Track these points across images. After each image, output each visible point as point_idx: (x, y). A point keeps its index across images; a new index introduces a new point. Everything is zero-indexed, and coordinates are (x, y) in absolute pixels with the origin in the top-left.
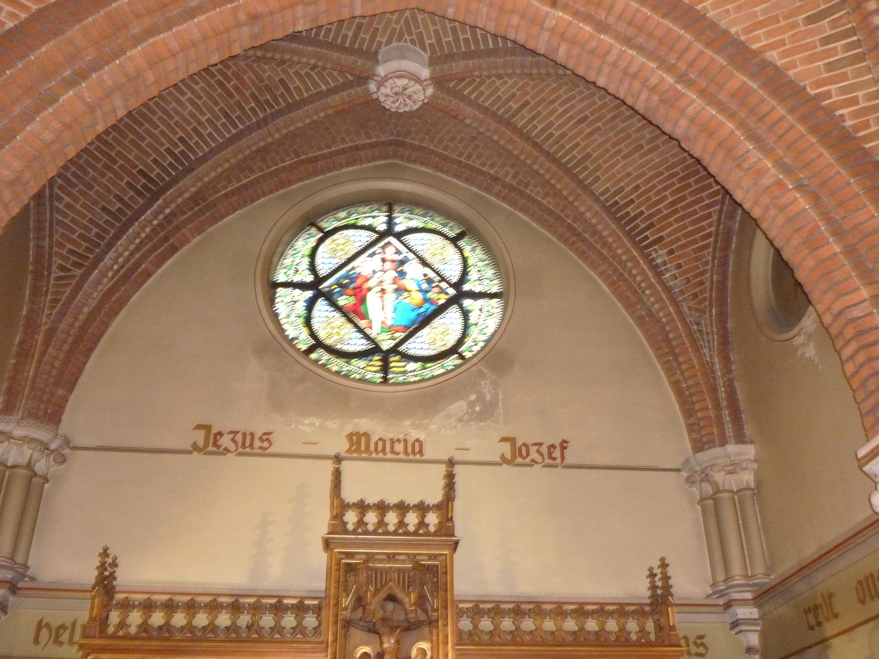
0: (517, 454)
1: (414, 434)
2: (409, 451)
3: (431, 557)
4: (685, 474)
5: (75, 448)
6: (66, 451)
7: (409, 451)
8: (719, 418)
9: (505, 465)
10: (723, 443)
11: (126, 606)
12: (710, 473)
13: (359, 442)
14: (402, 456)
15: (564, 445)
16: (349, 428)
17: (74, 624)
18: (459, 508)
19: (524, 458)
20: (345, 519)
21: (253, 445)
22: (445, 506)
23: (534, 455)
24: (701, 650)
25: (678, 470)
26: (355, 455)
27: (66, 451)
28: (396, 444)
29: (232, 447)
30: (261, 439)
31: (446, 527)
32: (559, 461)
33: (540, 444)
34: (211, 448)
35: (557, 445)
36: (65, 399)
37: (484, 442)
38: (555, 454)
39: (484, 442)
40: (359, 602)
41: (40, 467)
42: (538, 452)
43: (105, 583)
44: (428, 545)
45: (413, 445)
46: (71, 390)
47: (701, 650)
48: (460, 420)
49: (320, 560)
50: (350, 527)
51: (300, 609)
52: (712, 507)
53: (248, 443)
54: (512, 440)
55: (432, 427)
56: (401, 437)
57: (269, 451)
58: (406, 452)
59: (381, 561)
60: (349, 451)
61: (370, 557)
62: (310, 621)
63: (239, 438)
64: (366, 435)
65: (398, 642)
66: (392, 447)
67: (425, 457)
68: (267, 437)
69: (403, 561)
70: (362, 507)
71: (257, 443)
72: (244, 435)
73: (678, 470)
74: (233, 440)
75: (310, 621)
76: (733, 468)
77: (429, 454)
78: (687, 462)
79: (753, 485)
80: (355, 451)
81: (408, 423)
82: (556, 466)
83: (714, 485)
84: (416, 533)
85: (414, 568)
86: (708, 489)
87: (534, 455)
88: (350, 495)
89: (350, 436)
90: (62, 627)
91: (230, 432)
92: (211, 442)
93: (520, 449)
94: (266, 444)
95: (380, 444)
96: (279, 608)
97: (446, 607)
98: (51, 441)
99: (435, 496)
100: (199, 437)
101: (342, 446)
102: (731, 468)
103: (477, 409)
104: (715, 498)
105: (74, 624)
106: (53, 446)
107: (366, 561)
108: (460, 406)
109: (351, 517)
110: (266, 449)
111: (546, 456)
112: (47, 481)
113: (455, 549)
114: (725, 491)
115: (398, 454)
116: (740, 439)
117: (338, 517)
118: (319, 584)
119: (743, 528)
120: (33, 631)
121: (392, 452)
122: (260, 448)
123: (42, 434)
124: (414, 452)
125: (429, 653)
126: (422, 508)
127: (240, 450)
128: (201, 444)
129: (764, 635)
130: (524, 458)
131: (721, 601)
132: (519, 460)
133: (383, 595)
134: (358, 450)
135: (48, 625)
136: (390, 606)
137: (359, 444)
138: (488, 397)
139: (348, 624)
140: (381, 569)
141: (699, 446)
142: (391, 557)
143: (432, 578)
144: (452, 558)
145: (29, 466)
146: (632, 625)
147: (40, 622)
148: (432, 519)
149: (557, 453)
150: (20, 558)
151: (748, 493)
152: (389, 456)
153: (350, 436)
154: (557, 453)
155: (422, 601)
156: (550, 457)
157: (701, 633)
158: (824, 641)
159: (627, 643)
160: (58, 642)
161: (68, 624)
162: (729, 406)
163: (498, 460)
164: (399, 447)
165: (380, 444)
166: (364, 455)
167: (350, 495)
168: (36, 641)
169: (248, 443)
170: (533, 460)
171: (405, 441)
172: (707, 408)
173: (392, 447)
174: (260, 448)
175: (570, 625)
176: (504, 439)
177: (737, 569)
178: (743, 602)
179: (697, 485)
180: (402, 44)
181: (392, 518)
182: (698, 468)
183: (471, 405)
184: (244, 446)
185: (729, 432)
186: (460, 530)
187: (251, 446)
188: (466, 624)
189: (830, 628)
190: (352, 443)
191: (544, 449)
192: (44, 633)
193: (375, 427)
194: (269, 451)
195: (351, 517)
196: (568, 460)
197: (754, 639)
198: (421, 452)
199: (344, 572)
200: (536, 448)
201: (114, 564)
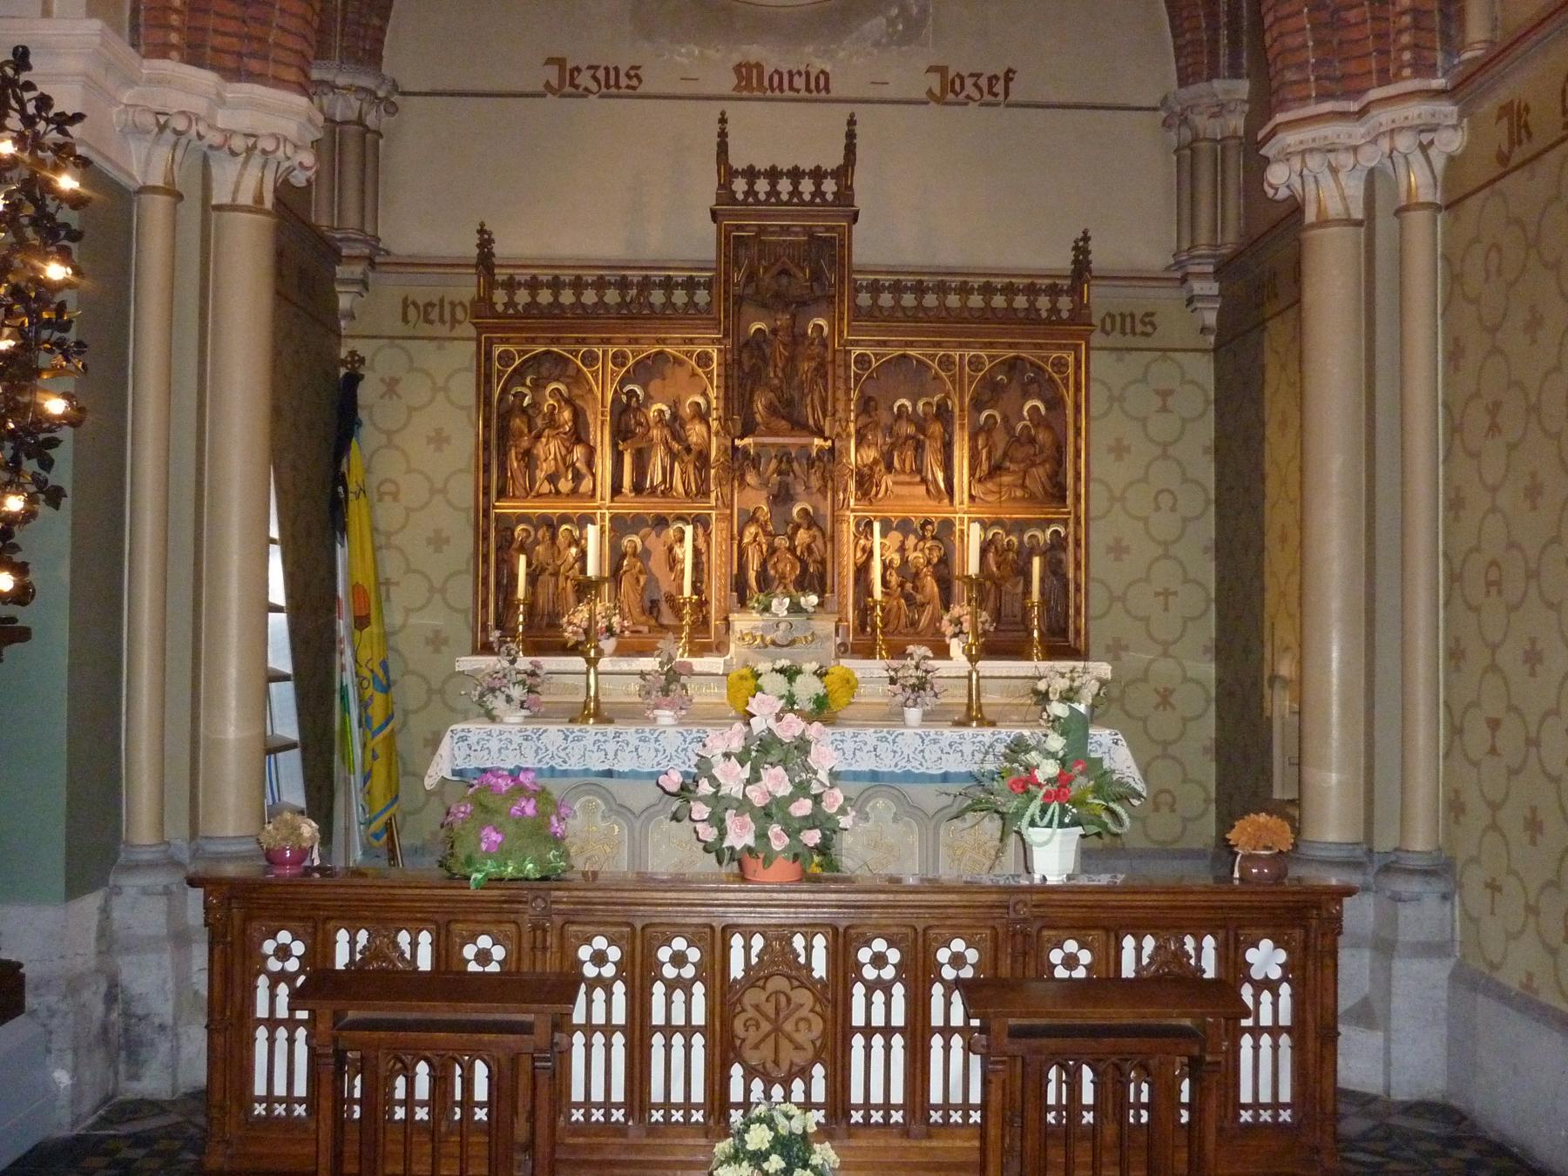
0: (950, 89)
1: (818, 64)
2: (813, 85)
3: (828, 229)
4: (1163, 114)
5: (404, 94)
6: (395, 98)
7: (813, 85)
8: (1214, 41)
9: (932, 104)
10: (1214, 74)
11: (511, 285)
12: (1191, 116)
13: (749, 79)
14: (803, 93)
15: (1009, 75)
16: (736, 58)
17: (442, 301)
18: (861, 180)
19: (957, 94)
20: (734, 187)
21: (617, 83)
22: (844, 173)
23: (970, 89)
24: (1149, 329)
25: (1155, 109)
26: (745, 94)
27: (395, 98)
28: (796, 78)
29: (593, 86)
30: (628, 76)
31: (845, 195)
32: (1001, 98)
33: (978, 76)
34: (568, 89)
35: (1001, 75)
36: (382, 30)
37: (908, 73)
38: (996, 88)
39: (908, 73)
40: (751, 277)
41: (370, 120)
42: (976, 85)
43: (485, 260)
44: (825, 217)
45: (817, 78)
46: (385, 18)
47: (1149, 329)
48: (877, 44)
49: (708, 231)
50: (740, 196)
51: (691, 285)
52: (1187, 155)
53: (612, 82)
54: (941, 70)
55: (841, 54)
56: (803, 68)
57: (640, 91)
58: (808, 89)
59: (773, 233)
60: (737, 88)
61: (762, 230)
62: (702, 296)
63: (601, 74)
64: (759, 66)
65: (794, 317)
66: (791, 81)
67: (833, 94)
68: (635, 73)
69: (796, 234)
70: (751, 174)
71: (624, 81)
72: (607, 69)
73: (1155, 109)
74: (595, 78)
75: (702, 296)
76: (1220, 110)
77: (837, 89)
78: (1165, 100)
79: (1241, 132)
80: (745, 88)
81: (809, 49)
82: (997, 105)
83: (1194, 129)
84: (812, 203)
85: (809, 243)
86: (1187, 134)
87: (970, 89)
88: (738, 161)
89: (738, 68)
90: (430, 304)
91: (590, 67)
92: (567, 81)
93: (953, 82)
94: (634, 82)
95: (776, 78)
96: (668, 285)
97: (842, 282)
98: (378, 87)
99: (834, 160)
100: (552, 74)
101: (728, 83)
102: (1216, 109)
103: (900, 27)
104: (1191, 146)
105: (442, 301)
106: (381, 94)
107: (758, 234)
108: (875, 25)
109: (740, 186)
110: (634, 88)
111: (985, 89)
112: (381, 136)
113: (855, 220)
114: (1206, 139)
115: (798, 91)
116: (1235, 73)
117: (725, 186)
118: (709, 252)
119: (1219, 185)
120: (400, 310)
121: (791, 88)
122: (628, 87)
123: (367, 82)
124: (818, 87)
125: (826, 330)
126: (818, 175)
127: (604, 90)
128: (555, 83)
129: (1221, 314)
130: (957, 94)
131: (1178, 275)
132: (951, 96)
133: (774, 271)
134: (749, 87)
135: (415, 304)
136: (784, 280)
137: (750, 80)
138: (915, 10)
139: (739, 300)
140: (771, 242)
141: (1183, 81)
142: (785, 230)
143: (827, 253)
144: (850, 231)
145: (360, 122)
146: (1043, 302)
147: (405, 300)
148: (829, 186)
149: (999, 88)
150: (369, 229)
151: (1233, 142)
152: (788, 93)
153: (738, 68)
154: (999, 88)
155: (817, 276)
156: (991, 92)
157: (1150, 310)
158: (1264, 321)
159: (1038, 321)
160: (428, 321)
161: (436, 301)
162: (1229, 25)
163: (924, 96)
164: (799, 82)
165: (776, 78)
166: (757, 94)
167: (738, 161)
168: (405, 320)
169: (612, 82)
170: (968, 97)
171: (808, 75)
172: (1198, 28)
173: (791, 81)
174: (628, 87)
175: (976, 301)
176: (931, 69)
177: (1204, 236)
178: (1201, 276)
179: (1175, 130)
180: (700, 371)
181: (784, 186)
182: (1178, 109)
183: (892, 22)
184: (608, 86)
185: (1224, 60)
186: (860, 202)
187: (617, 86)
188: (864, 299)
189: (1269, 310)
190: (740, 77)
191: (983, 82)
192: (412, 312)
193: (770, 56)
194: (640, 91)
195: (740, 186)
196: (1012, 98)
197: (1211, 318)
198: (827, 89)
199: (732, 245)
200: (973, 80)
201: (491, 241)
